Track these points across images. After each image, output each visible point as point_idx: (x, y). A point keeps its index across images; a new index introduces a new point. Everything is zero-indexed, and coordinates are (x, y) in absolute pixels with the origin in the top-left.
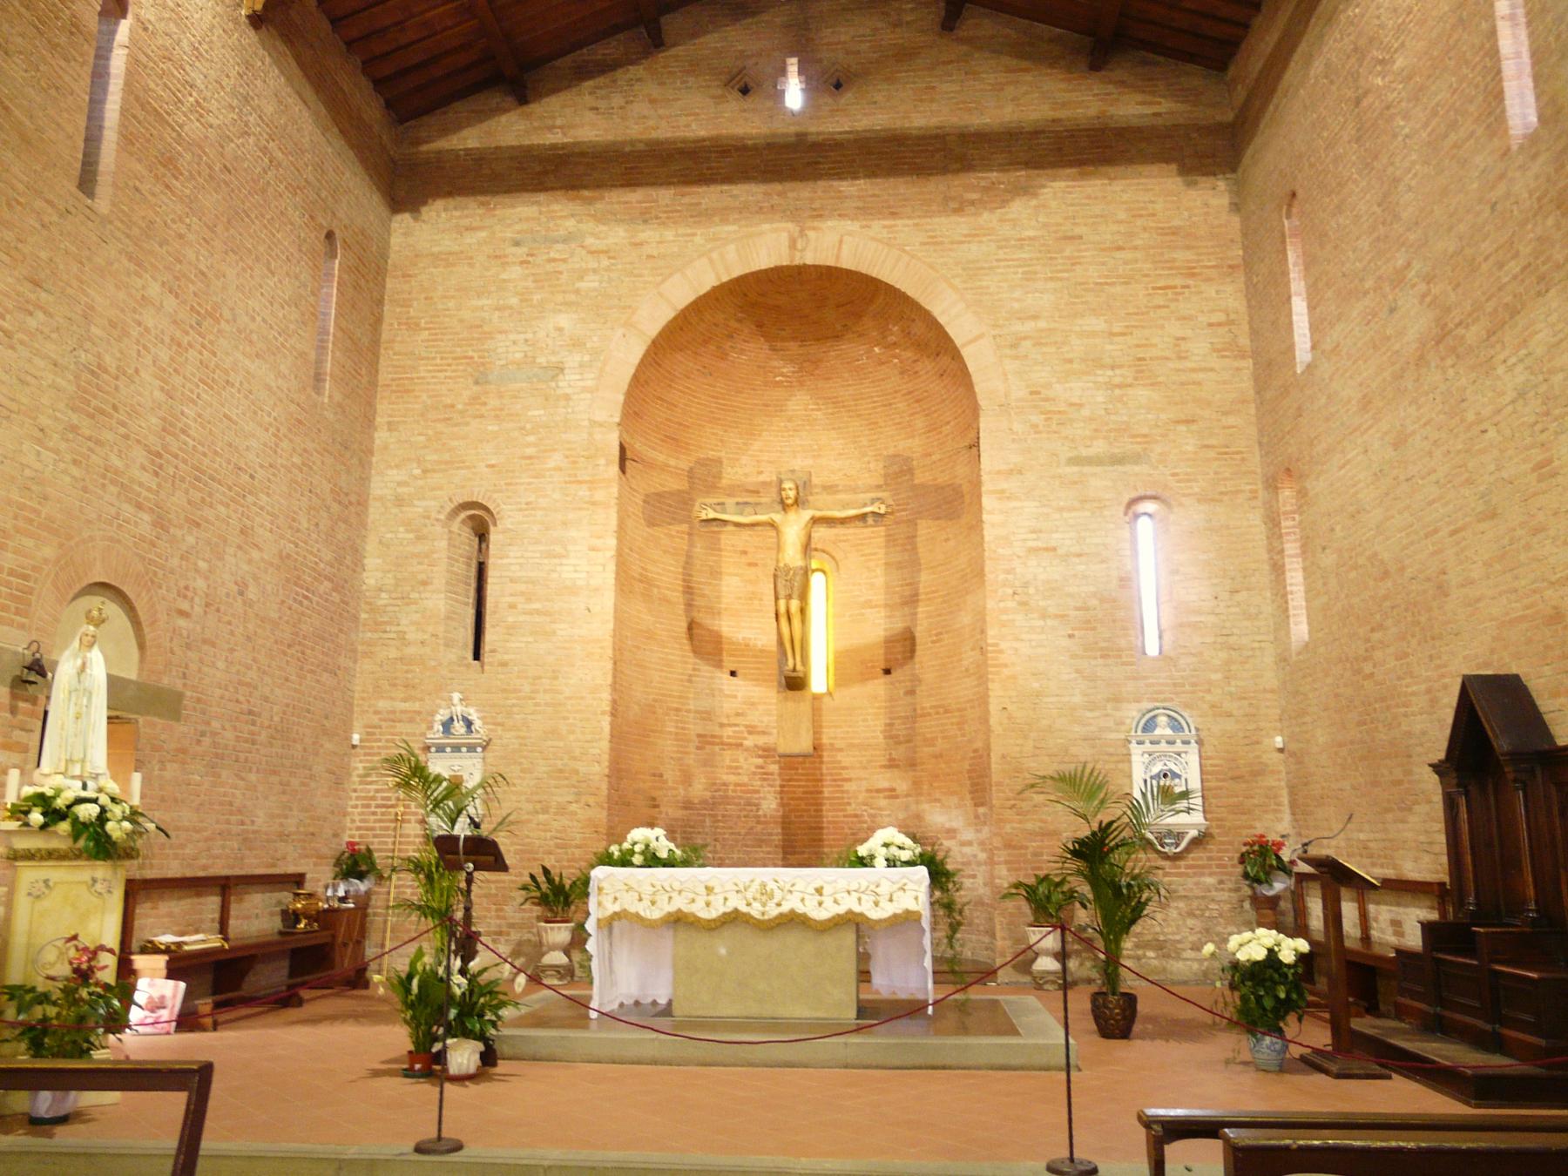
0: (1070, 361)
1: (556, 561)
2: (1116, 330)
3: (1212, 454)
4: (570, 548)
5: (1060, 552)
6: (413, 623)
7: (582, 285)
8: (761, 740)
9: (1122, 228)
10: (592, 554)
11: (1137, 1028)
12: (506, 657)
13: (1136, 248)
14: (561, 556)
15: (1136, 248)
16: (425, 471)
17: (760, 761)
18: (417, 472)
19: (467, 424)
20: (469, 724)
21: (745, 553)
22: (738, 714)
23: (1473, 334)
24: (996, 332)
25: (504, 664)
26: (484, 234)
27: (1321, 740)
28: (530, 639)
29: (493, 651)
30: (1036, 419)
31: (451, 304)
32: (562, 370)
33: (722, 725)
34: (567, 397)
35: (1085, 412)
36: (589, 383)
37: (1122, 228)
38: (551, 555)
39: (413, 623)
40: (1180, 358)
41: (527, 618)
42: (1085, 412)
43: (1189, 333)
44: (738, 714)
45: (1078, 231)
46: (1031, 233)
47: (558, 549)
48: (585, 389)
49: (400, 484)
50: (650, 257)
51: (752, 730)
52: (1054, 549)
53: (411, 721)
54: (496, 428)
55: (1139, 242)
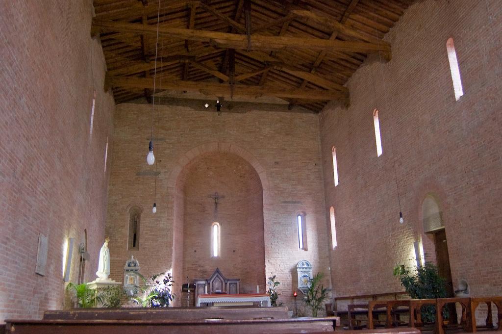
0: (283, 179)
1: (158, 222)
2: (294, 171)
3: (315, 202)
4: (162, 219)
5: (281, 223)
6: (119, 237)
7: (165, 152)
8: (202, 269)
9: (296, 148)
10: (168, 221)
11: (317, 316)
12: (145, 246)
13: (298, 153)
14: (159, 221)
15: (298, 153)
16: (123, 197)
17: (202, 274)
18: (121, 197)
19: (134, 185)
20: (135, 265)
21: (198, 220)
22: (196, 262)
23: (372, 188)
24: (18, 13)
25: (144, 248)
26: (139, 136)
27: (340, 268)
28: (151, 242)
29: (141, 245)
30: (276, 192)
31: (130, 154)
32: (160, 173)
33: (193, 265)
34: (161, 180)
35: (287, 191)
36: (167, 177)
37: (296, 148)
38: (157, 220)
39: (119, 237)
40: (308, 179)
41: (151, 237)
42: (287, 191)
43: (310, 173)
44: (196, 262)
45: (285, 148)
46: (275, 147)
47: (159, 219)
48: (165, 178)
49: (116, 200)
50: (183, 146)
51: (200, 266)
52: (280, 223)
53: (119, 262)
54: (142, 187)
55: (299, 152)
